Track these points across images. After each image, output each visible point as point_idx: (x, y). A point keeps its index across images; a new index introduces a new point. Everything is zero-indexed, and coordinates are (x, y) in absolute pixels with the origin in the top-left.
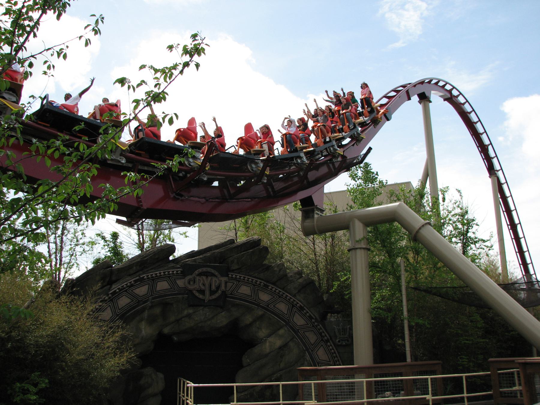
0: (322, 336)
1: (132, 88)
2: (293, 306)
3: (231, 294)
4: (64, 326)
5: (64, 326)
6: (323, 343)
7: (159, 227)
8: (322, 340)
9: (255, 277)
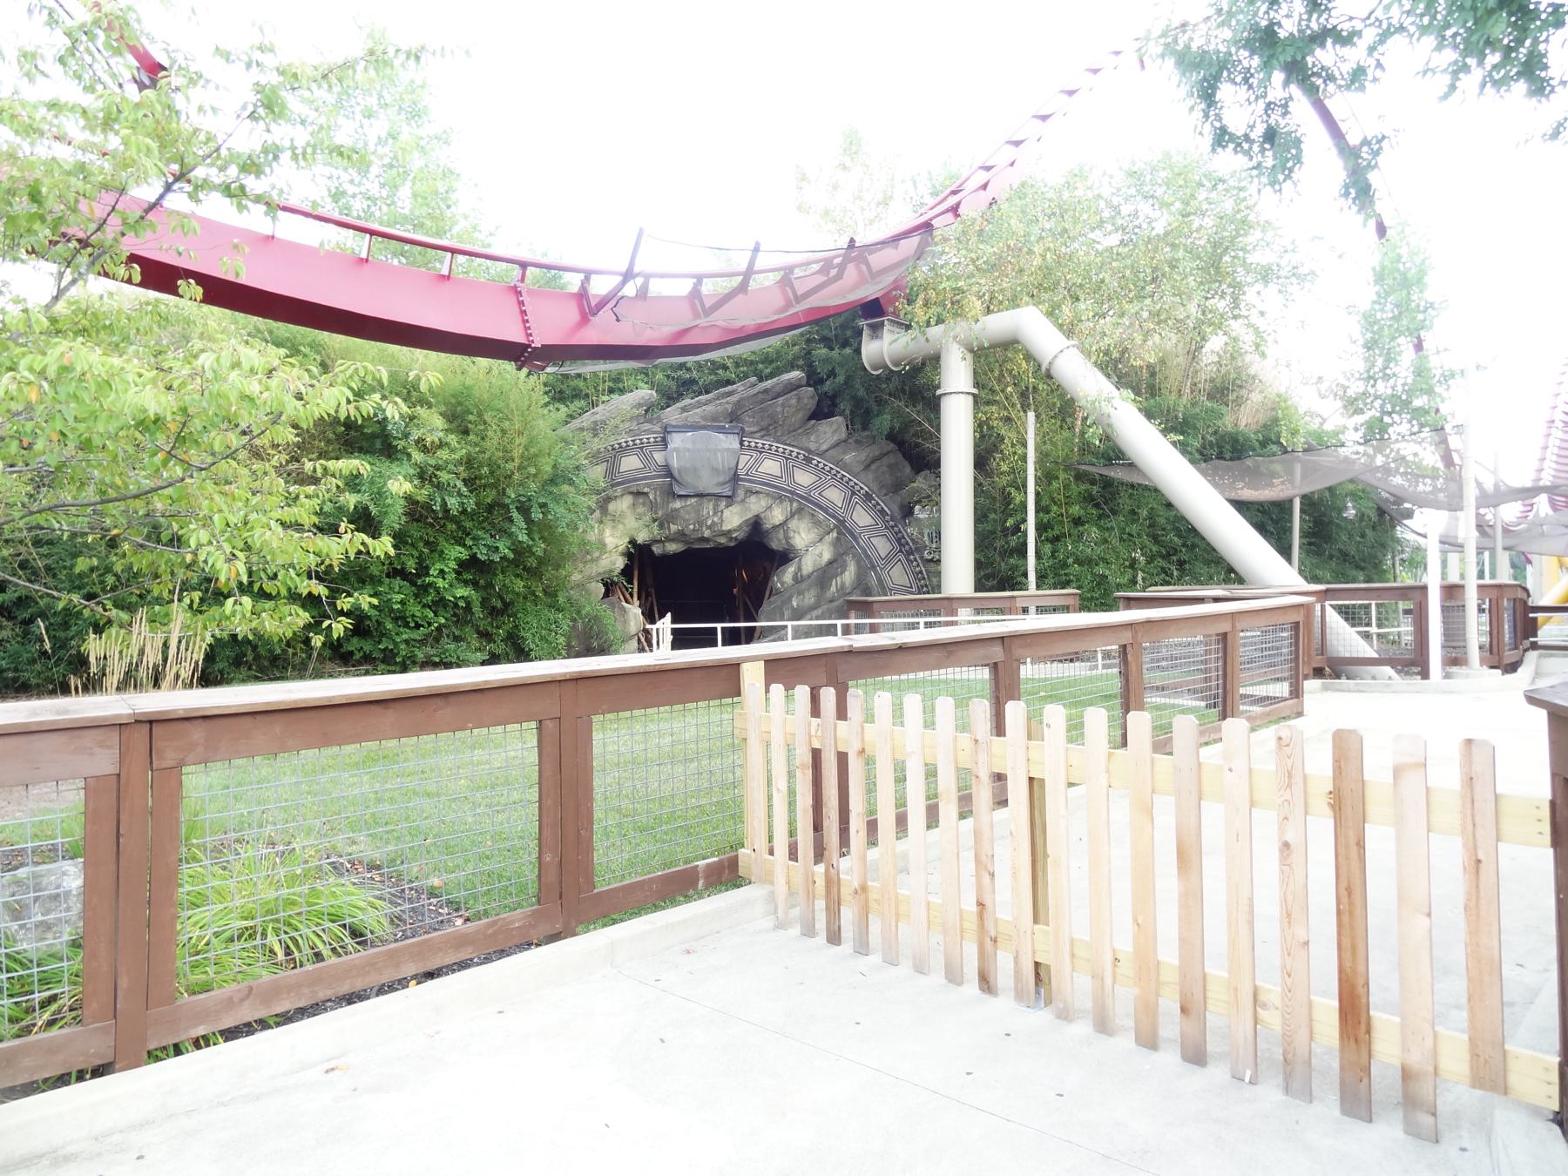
0: (901, 545)
1: (413, 58)
2: (853, 493)
3: (747, 474)
4: (154, 381)
5: (154, 381)
6: (901, 557)
7: (373, 436)
8: (901, 551)
9: (789, 445)
